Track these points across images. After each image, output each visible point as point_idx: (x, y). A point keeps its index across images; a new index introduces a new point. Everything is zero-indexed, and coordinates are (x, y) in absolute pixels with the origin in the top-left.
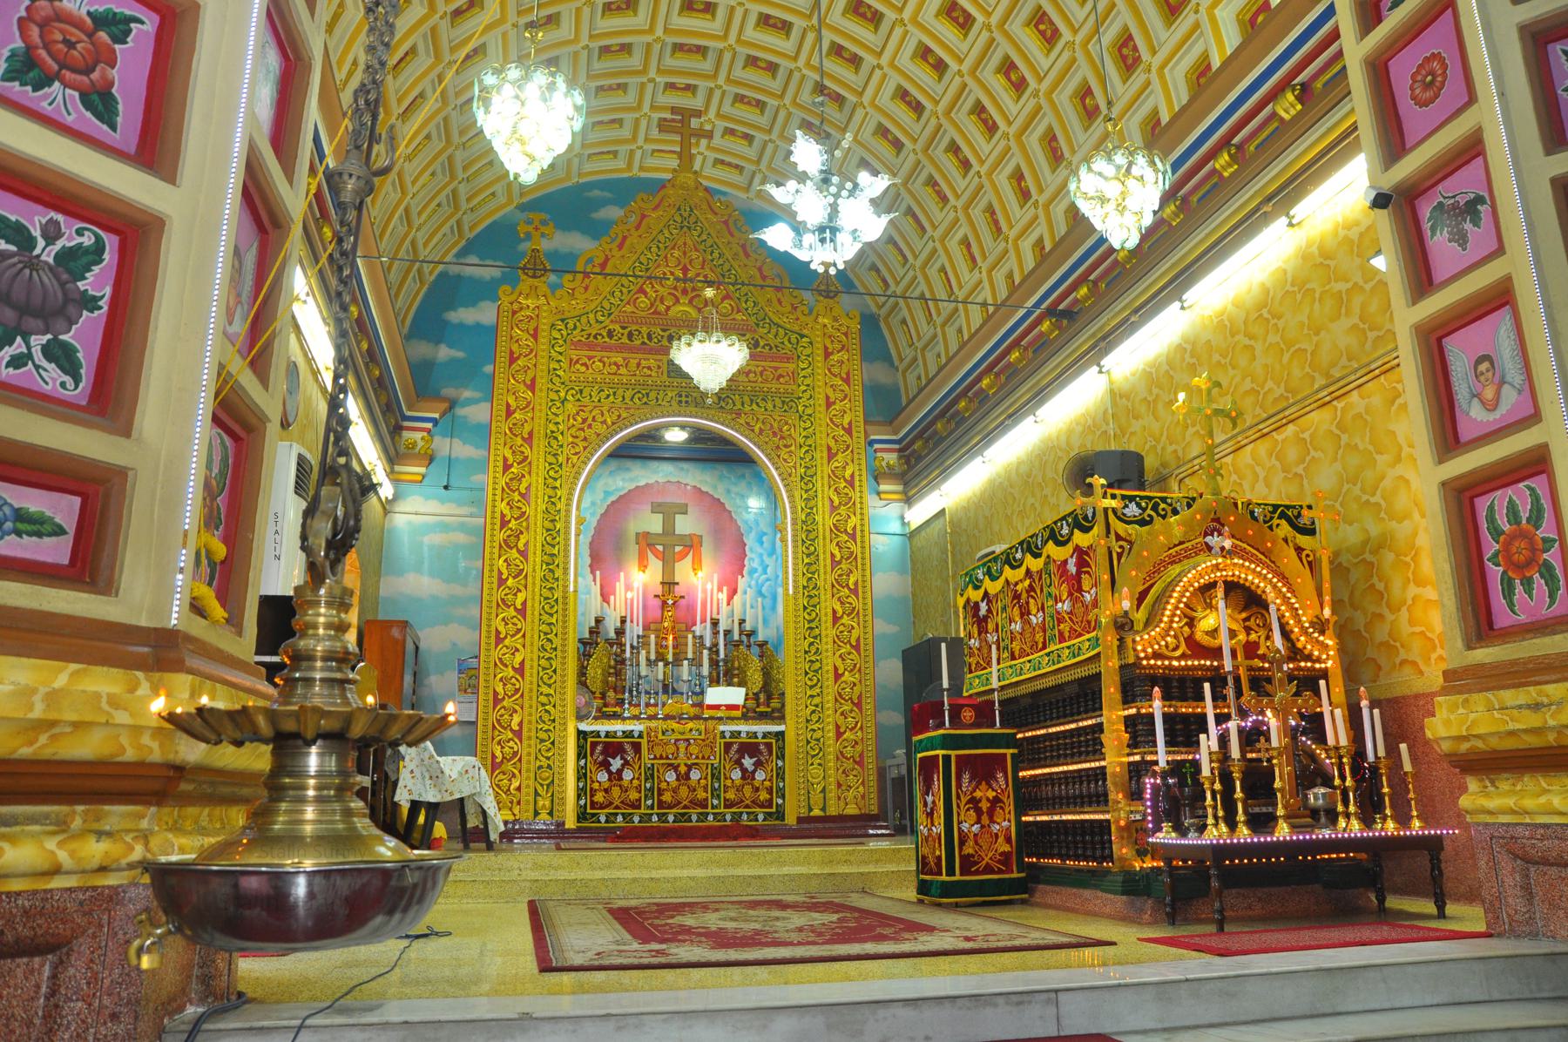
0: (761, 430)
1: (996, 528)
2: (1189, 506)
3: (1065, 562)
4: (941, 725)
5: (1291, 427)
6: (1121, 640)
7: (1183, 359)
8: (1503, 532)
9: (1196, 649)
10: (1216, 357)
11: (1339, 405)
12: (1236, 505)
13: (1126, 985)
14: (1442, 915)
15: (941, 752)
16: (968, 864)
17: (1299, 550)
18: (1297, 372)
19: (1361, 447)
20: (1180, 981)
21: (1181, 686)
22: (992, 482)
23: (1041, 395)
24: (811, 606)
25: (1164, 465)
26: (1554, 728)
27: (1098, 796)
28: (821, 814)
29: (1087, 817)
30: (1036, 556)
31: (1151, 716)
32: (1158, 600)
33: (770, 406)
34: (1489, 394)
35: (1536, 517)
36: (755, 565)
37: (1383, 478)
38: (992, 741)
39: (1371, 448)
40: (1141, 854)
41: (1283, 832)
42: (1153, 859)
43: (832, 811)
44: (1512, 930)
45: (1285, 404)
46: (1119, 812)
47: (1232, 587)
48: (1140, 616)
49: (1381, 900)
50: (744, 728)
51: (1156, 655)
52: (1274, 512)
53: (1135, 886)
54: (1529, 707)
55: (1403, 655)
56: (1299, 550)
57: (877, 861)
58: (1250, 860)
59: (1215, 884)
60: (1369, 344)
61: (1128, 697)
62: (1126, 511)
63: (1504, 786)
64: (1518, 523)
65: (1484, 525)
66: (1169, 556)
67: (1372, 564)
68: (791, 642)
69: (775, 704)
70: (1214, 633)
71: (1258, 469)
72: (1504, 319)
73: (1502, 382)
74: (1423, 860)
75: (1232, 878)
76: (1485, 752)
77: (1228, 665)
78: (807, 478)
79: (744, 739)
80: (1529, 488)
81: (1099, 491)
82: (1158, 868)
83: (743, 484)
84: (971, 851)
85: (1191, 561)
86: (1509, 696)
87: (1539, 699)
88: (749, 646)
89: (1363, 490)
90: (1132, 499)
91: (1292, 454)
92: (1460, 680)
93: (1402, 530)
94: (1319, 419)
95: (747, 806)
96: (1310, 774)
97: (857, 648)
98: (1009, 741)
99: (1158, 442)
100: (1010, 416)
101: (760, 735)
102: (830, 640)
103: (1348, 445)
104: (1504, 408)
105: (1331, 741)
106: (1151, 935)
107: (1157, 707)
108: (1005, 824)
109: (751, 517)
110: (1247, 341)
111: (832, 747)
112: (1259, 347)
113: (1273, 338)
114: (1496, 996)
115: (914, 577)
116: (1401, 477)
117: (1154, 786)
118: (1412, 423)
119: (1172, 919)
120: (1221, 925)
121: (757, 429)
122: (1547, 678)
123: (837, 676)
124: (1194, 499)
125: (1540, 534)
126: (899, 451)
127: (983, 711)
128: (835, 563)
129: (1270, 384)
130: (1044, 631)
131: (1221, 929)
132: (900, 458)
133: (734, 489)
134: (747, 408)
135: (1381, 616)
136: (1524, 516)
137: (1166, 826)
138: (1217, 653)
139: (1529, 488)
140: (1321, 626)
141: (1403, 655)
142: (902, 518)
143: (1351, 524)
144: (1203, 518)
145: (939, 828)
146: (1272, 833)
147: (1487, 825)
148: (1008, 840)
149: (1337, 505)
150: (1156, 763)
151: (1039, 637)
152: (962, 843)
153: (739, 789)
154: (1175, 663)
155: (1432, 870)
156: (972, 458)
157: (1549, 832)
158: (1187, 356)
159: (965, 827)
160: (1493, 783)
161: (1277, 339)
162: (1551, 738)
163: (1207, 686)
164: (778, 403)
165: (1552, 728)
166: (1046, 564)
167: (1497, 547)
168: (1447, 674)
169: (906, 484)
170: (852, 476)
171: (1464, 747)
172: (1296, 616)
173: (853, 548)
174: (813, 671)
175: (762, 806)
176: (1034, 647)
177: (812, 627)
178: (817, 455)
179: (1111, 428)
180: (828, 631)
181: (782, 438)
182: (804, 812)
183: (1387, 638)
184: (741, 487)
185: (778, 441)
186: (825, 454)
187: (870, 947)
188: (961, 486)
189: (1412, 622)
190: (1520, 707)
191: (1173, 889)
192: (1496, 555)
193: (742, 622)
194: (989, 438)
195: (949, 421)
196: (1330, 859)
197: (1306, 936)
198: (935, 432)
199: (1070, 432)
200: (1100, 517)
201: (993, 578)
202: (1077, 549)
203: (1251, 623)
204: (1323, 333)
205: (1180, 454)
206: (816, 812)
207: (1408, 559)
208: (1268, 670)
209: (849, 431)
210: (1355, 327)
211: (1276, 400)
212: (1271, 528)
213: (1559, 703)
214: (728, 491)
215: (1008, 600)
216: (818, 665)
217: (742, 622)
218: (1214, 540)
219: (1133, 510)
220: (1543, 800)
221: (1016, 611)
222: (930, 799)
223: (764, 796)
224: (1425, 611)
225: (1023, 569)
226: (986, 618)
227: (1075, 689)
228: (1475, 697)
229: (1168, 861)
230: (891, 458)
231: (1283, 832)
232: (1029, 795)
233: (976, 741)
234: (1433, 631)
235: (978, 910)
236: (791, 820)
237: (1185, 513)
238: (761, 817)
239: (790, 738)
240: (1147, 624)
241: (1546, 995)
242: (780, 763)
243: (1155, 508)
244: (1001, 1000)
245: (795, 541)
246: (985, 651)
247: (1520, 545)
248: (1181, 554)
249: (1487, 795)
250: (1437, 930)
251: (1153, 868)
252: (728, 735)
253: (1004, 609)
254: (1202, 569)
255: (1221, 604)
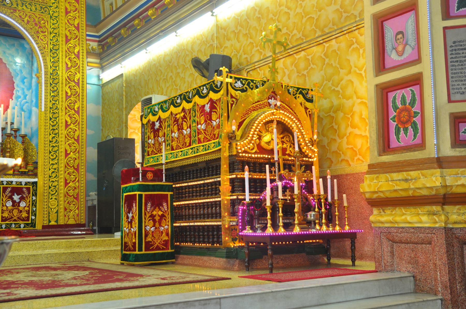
0: (28, 22)
1: (151, 86)
2: (263, 85)
3: (204, 106)
4: (138, 180)
5: (303, 52)
6: (230, 144)
7: (254, 14)
8: (398, 108)
9: (261, 150)
10: (271, 16)
11: (326, 45)
12: (282, 86)
13: (248, 295)
14: (354, 265)
15: (138, 193)
16: (149, 246)
17: (306, 108)
18: (308, 28)
19: (334, 65)
20: (269, 292)
21: (257, 167)
22: (149, 63)
23: (179, 23)
24: (54, 118)
25: (240, 64)
26: (412, 189)
27: (216, 214)
28: (56, 224)
29: (206, 224)
30: (188, 102)
31: (243, 180)
32: (247, 126)
33: (33, 8)
34: (400, 48)
35: (413, 103)
36: (20, 94)
37: (342, 80)
38: (162, 188)
39: (338, 66)
40: (234, 240)
41: (297, 230)
42: (239, 242)
43: (61, 222)
44: (385, 269)
45: (301, 42)
46: (227, 221)
47: (280, 123)
48: (239, 133)
49: (329, 260)
50: (14, 179)
51: (245, 152)
52: (297, 91)
53: (231, 254)
54: (403, 180)
55: (343, 157)
56: (306, 108)
57: (94, 246)
58: (286, 243)
59: (270, 252)
60: (342, 20)
61: (232, 170)
62: (236, 85)
63: (388, 212)
64: (405, 105)
65: (391, 104)
66: (253, 107)
67: (333, 117)
68: (43, 136)
69: (30, 167)
70: (268, 143)
71: (286, 70)
72: (411, 17)
73: (406, 44)
74: (348, 243)
75: (278, 251)
76: (383, 198)
77: (276, 159)
78: (54, 51)
79: (14, 185)
80: (411, 90)
81: (224, 74)
82: (243, 247)
83: (13, 49)
84: (150, 240)
85: (262, 110)
86: (395, 176)
87: (407, 177)
88: (16, 137)
89: (333, 85)
90: (239, 79)
91: (302, 65)
92: (374, 168)
93: (348, 103)
94: (317, 50)
95: (15, 220)
96: (307, 208)
97: (77, 141)
98: (170, 188)
99: (239, 53)
100: (162, 31)
101: (23, 184)
102: (63, 136)
103: (328, 64)
104: (405, 55)
105: (315, 192)
106: (244, 275)
107: (246, 175)
108: (166, 227)
109: (18, 68)
110: (286, 10)
111: (62, 190)
112: (292, 13)
113: (299, 10)
114: (382, 294)
115: (103, 107)
116: (350, 81)
117: (243, 209)
118: (365, 59)
119: (248, 268)
120: (271, 270)
121: (26, 20)
122: (411, 169)
123: (67, 154)
124: (265, 82)
125: (413, 110)
126: (99, 41)
127: (157, 174)
128: (67, 97)
129: (295, 32)
130: (190, 137)
131: (271, 272)
132: (99, 45)
133: (8, 52)
134: (20, 8)
135: (335, 140)
136: (408, 102)
137: (248, 227)
138: (271, 152)
139: (411, 90)
140: (312, 142)
141: (343, 157)
142: (99, 76)
143: (326, 99)
144: (269, 91)
145: (135, 228)
146: (292, 231)
147: (380, 227)
148: (167, 234)
149: (320, 90)
150: (245, 199)
151: (187, 141)
152: (146, 236)
153: (11, 211)
154: (253, 156)
155: (352, 246)
156: (140, 50)
157: (404, 230)
158: (257, 13)
159: (148, 228)
160: (384, 211)
161: (301, 11)
162: (410, 193)
163: (267, 166)
164: (38, 7)
165: (412, 189)
166: (194, 106)
167: (395, 114)
168: (370, 166)
169: (101, 59)
170: (79, 52)
171: (375, 196)
172: (303, 137)
173: (78, 90)
174: (53, 152)
175: (23, 220)
176: (184, 145)
177: (54, 129)
178: (60, 39)
179: (215, 43)
180: (63, 132)
181: (40, 27)
182: (46, 223)
183: (336, 149)
184: (12, 51)
185: (38, 29)
186: (64, 39)
187: (118, 285)
188: (133, 63)
189: (348, 143)
190: (399, 180)
191: (249, 254)
192: (394, 117)
193: (12, 123)
194: (150, 41)
195: (128, 29)
196: (309, 242)
197: (308, 274)
198: (120, 34)
199: (193, 43)
200: (224, 85)
201: (164, 111)
202: (211, 100)
203: (284, 140)
204: (323, 11)
205: (249, 60)
206: (53, 223)
207: (349, 116)
208: (293, 161)
209: (77, 28)
210: (338, 10)
211: (297, 40)
212: (295, 98)
213: (415, 179)
214: (5, 52)
215: (171, 122)
216: (56, 149)
217: (12, 123)
218: (272, 101)
219: (239, 84)
220: (403, 217)
221: (176, 128)
222: (130, 215)
223: (24, 215)
224: (359, 139)
225: (181, 108)
226: (158, 130)
227: (204, 165)
228: (381, 175)
229: (247, 243)
230: (94, 45)
231: (297, 230)
232: (177, 214)
233: (154, 188)
234: (356, 148)
235: (149, 267)
236: (39, 227)
237: (261, 88)
238: (22, 226)
239: (40, 185)
240: (242, 137)
241: (397, 293)
242: (34, 198)
243: (248, 84)
244: (197, 303)
245: (46, 83)
246: (157, 145)
247: (405, 114)
248: (259, 106)
249: (381, 216)
250: (356, 270)
251: (239, 246)
252: (5, 183)
253: (169, 126)
254: (267, 114)
255: (275, 130)
